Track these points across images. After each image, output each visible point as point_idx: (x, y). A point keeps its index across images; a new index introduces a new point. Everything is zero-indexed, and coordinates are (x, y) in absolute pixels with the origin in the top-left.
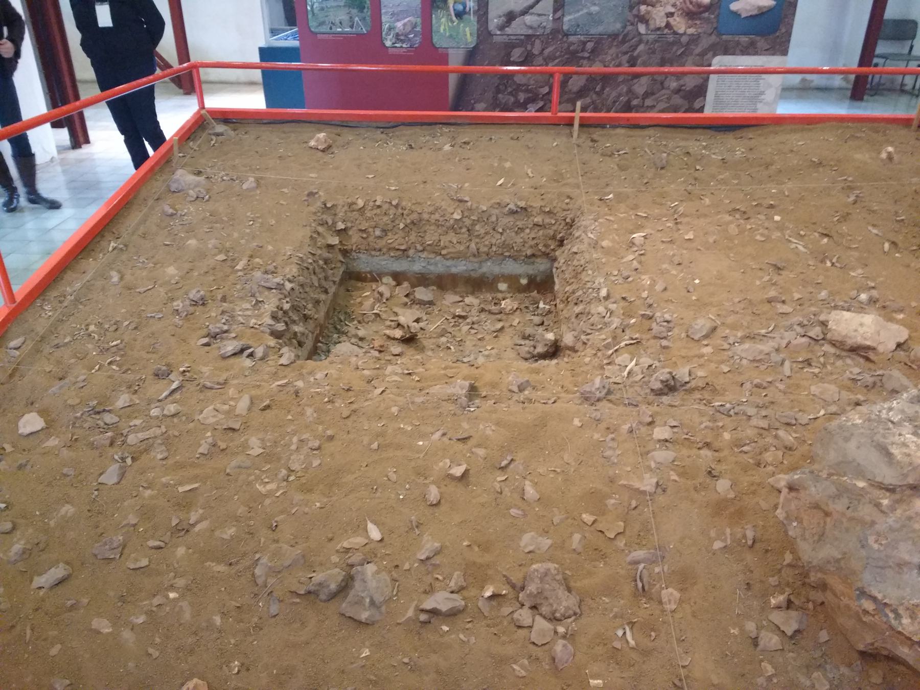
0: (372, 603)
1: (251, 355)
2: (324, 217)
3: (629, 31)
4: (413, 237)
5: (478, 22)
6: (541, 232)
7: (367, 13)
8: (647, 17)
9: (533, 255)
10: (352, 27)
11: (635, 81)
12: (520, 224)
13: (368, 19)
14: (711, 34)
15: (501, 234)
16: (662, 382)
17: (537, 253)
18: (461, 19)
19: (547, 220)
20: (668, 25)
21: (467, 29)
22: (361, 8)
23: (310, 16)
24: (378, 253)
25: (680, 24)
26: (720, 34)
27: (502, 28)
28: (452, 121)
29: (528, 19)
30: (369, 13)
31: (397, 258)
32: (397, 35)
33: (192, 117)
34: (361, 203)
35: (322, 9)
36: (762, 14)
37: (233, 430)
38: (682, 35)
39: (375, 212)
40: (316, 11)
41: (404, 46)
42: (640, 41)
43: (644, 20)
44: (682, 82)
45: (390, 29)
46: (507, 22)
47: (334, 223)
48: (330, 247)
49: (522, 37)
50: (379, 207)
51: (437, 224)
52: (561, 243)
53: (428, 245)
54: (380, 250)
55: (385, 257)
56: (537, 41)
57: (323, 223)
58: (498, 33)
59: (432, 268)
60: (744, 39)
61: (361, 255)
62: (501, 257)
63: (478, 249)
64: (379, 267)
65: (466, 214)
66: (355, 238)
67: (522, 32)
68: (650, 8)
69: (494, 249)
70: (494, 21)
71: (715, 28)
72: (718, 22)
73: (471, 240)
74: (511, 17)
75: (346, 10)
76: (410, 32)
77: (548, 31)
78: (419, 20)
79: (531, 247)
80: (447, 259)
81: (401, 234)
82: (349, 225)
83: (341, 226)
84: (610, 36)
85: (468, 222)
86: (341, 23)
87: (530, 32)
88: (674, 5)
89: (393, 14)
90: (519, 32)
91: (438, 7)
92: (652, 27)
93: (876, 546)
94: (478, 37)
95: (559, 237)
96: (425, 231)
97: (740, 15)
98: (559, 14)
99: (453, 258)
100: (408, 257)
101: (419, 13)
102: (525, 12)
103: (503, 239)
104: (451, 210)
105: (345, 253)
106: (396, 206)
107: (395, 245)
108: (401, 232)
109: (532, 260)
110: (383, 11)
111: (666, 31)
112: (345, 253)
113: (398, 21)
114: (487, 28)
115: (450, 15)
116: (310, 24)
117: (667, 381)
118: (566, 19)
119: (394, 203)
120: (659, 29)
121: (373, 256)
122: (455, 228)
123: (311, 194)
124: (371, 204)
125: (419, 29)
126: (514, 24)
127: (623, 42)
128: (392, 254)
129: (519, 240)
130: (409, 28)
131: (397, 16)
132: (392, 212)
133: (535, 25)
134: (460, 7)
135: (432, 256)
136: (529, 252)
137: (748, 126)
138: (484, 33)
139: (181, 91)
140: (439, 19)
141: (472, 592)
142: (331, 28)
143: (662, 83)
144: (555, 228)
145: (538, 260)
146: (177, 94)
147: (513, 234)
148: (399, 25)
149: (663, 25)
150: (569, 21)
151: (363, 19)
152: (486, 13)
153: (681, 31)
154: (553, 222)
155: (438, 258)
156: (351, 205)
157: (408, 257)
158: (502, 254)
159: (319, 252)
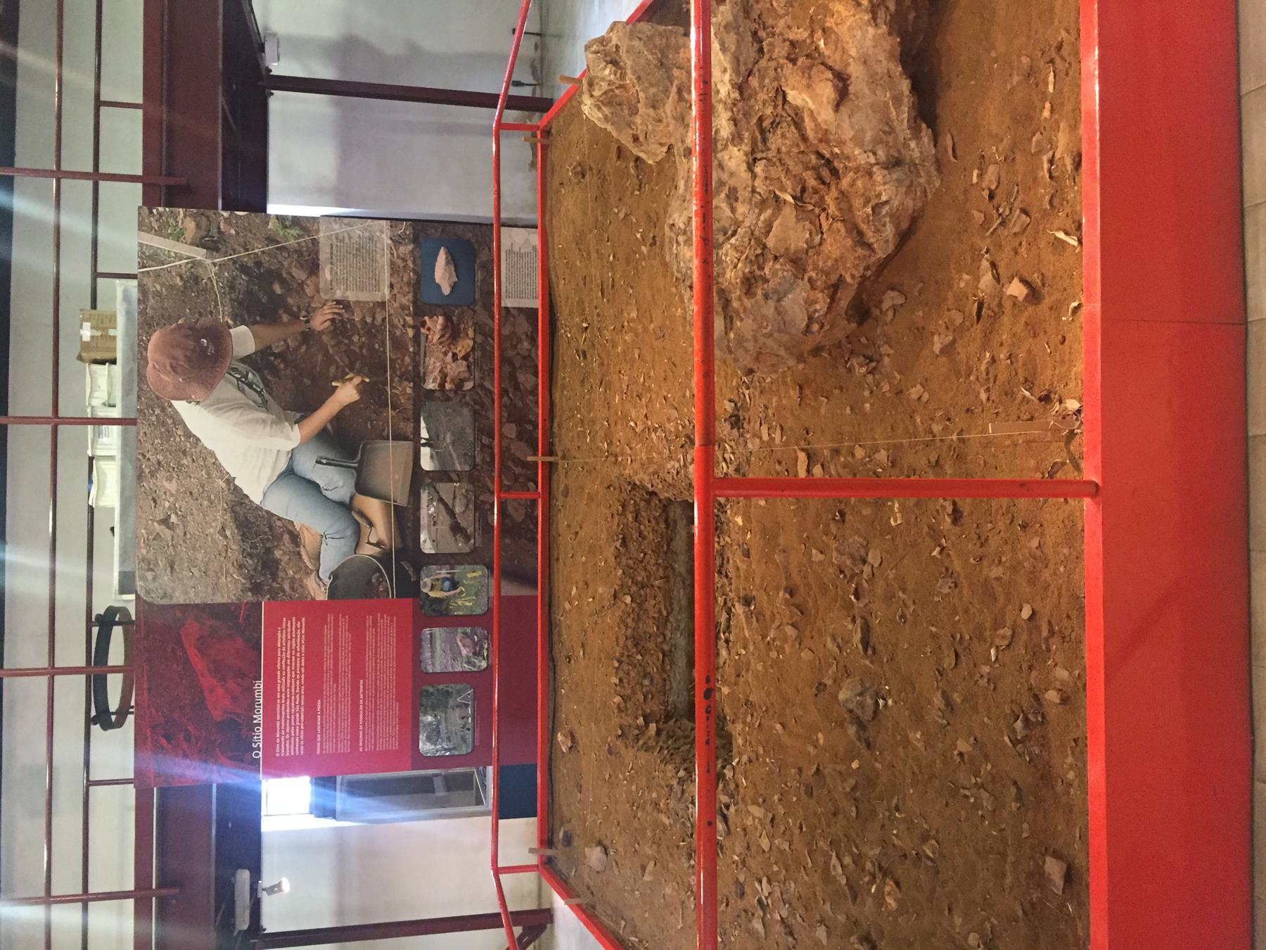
0: (861, 694)
1: (727, 807)
2: (631, 737)
3: (473, 400)
4: (650, 645)
5: (462, 564)
6: (643, 514)
7: (452, 687)
8: (457, 381)
9: (666, 521)
10: (467, 706)
11: (522, 388)
12: (635, 535)
13: (459, 686)
14: (475, 312)
15: (645, 554)
16: (732, 428)
17: (664, 517)
18: (458, 583)
19: (631, 508)
20: (465, 358)
21: (469, 576)
22: (448, 694)
23: (457, 753)
24: (668, 682)
25: (464, 346)
26: (474, 302)
27: (467, 538)
28: (547, 599)
29: (458, 510)
30: (453, 686)
31: (672, 662)
32: (475, 654)
33: (593, 933)
34: (617, 699)
35: (449, 739)
36: (453, 260)
37: (773, 820)
38: (475, 342)
39: (626, 685)
40: (451, 746)
41: (486, 646)
42: (482, 386)
43: (459, 384)
44: (523, 337)
45: (469, 663)
46: (462, 532)
47: (638, 727)
48: (658, 732)
49: (477, 514)
50: (621, 680)
51: (637, 620)
52: (653, 494)
53: (658, 629)
54: (665, 680)
55: (672, 675)
56: (481, 498)
57: (637, 738)
58: (472, 541)
59: (682, 626)
60: (479, 276)
61: (671, 700)
62: (669, 554)
63: (661, 578)
64: (682, 683)
65: (626, 590)
66: (653, 706)
67: (472, 515)
68: (448, 379)
69: (660, 561)
70: (460, 546)
71: (468, 306)
72: (461, 306)
73: (652, 586)
74: (456, 528)
75: (449, 711)
76: (473, 640)
77: (471, 487)
78: (460, 630)
79: (658, 523)
80: (672, 609)
81: (647, 657)
82: (640, 712)
83: (640, 721)
84: (475, 420)
85: (634, 589)
86: (463, 718)
87: (471, 506)
88: (445, 354)
89: (454, 659)
90: (471, 518)
91: (447, 608)
92: (466, 375)
93: (769, 328)
94: (477, 563)
95: (647, 497)
96: (645, 632)
97: (455, 283)
98: (454, 476)
99: (671, 604)
100: (671, 651)
101: (453, 629)
102: (451, 513)
103: (650, 552)
104: (623, 606)
105: (668, 717)
106: (620, 662)
107: (658, 664)
108: (646, 658)
109: (671, 523)
110: (450, 670)
111: (471, 359)
112: (668, 717)
113: (460, 653)
114: (467, 554)
115: (454, 595)
116: (464, 753)
117: (731, 424)
118: (458, 468)
119: (616, 665)
120: (469, 367)
121: (671, 688)
122: (639, 602)
123: (610, 751)
124: (618, 688)
125: (468, 630)
126: (463, 524)
127: (482, 405)
128: (668, 667)
129: (651, 536)
130: (468, 641)
131: (456, 655)
132: (626, 667)
133: (464, 501)
134: (447, 584)
135: (669, 626)
136: (663, 526)
137: (551, 301)
138: (472, 558)
139: (548, 925)
140: (459, 608)
141: (856, 611)
142: (468, 729)
143: (524, 358)
144: (638, 500)
145: (671, 515)
146: (552, 929)
147: (645, 542)
148: (464, 652)
149: (465, 363)
150: (460, 464)
151: (459, 692)
152: (452, 555)
153: (471, 343)
154: (632, 502)
155: (671, 619)
156: (620, 710)
157: (671, 651)
158: (666, 553)
159: (661, 744)
